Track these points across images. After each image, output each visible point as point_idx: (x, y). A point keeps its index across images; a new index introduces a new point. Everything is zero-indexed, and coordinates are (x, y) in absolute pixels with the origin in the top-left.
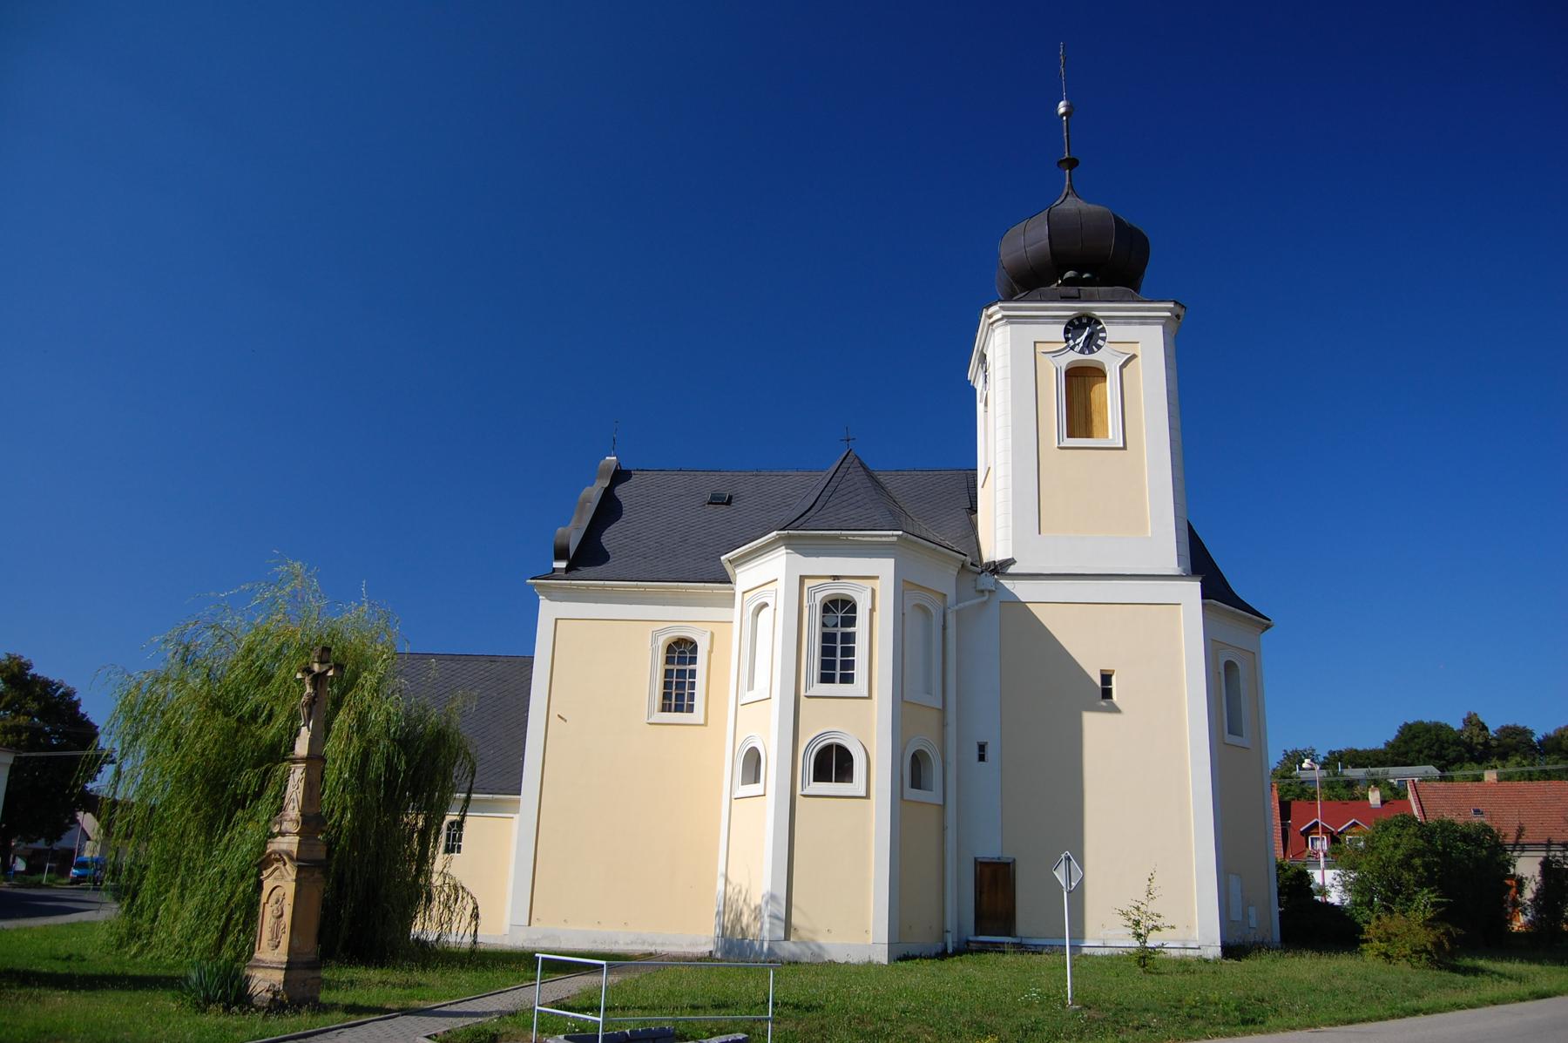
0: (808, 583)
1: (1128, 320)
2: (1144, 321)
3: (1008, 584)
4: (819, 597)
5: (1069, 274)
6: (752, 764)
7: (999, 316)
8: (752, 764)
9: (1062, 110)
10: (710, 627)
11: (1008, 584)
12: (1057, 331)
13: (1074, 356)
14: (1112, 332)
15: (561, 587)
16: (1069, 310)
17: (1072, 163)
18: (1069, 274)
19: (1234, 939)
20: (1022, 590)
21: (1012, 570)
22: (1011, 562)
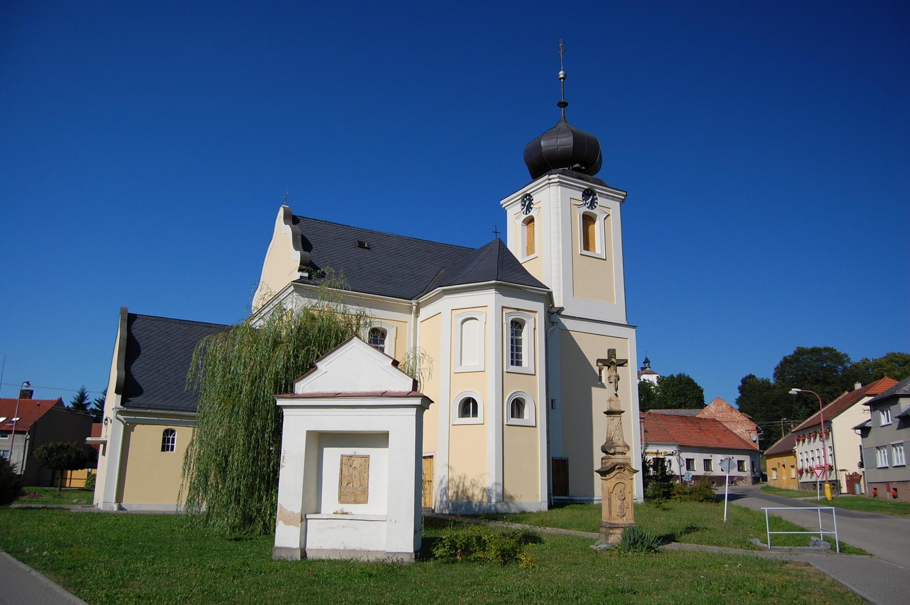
0: (505, 311)
1: (607, 197)
2: (613, 198)
3: (562, 320)
4: (511, 319)
5: (577, 165)
6: (468, 407)
7: (557, 180)
8: (468, 407)
9: (561, 74)
10: (395, 324)
11: (562, 320)
12: (579, 195)
13: (586, 209)
14: (600, 201)
15: (310, 290)
16: (585, 185)
17: (563, 105)
18: (577, 165)
19: (89, 494)
20: (568, 324)
21: (563, 313)
22: (562, 309)
